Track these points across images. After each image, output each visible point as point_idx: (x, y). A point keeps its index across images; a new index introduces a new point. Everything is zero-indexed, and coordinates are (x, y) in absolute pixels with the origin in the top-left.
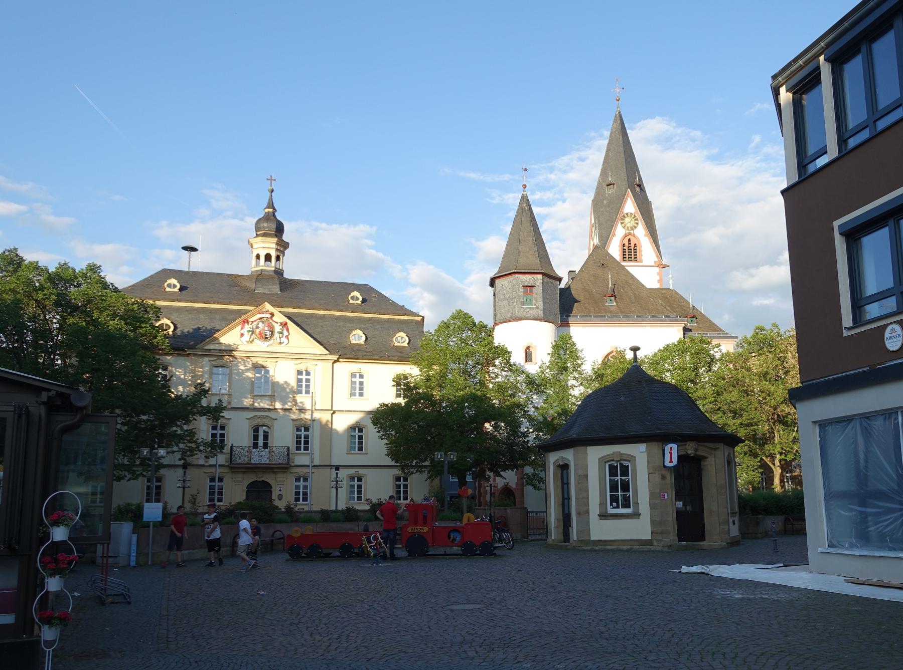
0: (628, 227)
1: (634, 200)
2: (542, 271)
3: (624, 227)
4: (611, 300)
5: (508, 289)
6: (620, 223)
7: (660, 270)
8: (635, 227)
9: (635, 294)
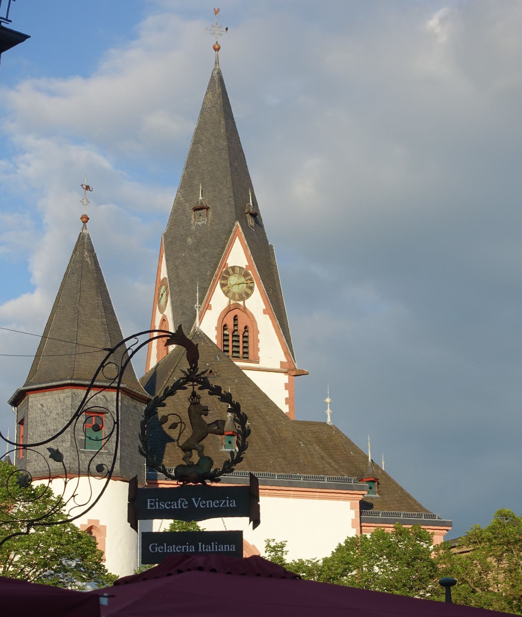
0: (234, 294)
1: (246, 242)
3: (226, 294)
4: (230, 442)
5: (54, 415)
6: (219, 285)
8: (248, 295)
9: (271, 433)
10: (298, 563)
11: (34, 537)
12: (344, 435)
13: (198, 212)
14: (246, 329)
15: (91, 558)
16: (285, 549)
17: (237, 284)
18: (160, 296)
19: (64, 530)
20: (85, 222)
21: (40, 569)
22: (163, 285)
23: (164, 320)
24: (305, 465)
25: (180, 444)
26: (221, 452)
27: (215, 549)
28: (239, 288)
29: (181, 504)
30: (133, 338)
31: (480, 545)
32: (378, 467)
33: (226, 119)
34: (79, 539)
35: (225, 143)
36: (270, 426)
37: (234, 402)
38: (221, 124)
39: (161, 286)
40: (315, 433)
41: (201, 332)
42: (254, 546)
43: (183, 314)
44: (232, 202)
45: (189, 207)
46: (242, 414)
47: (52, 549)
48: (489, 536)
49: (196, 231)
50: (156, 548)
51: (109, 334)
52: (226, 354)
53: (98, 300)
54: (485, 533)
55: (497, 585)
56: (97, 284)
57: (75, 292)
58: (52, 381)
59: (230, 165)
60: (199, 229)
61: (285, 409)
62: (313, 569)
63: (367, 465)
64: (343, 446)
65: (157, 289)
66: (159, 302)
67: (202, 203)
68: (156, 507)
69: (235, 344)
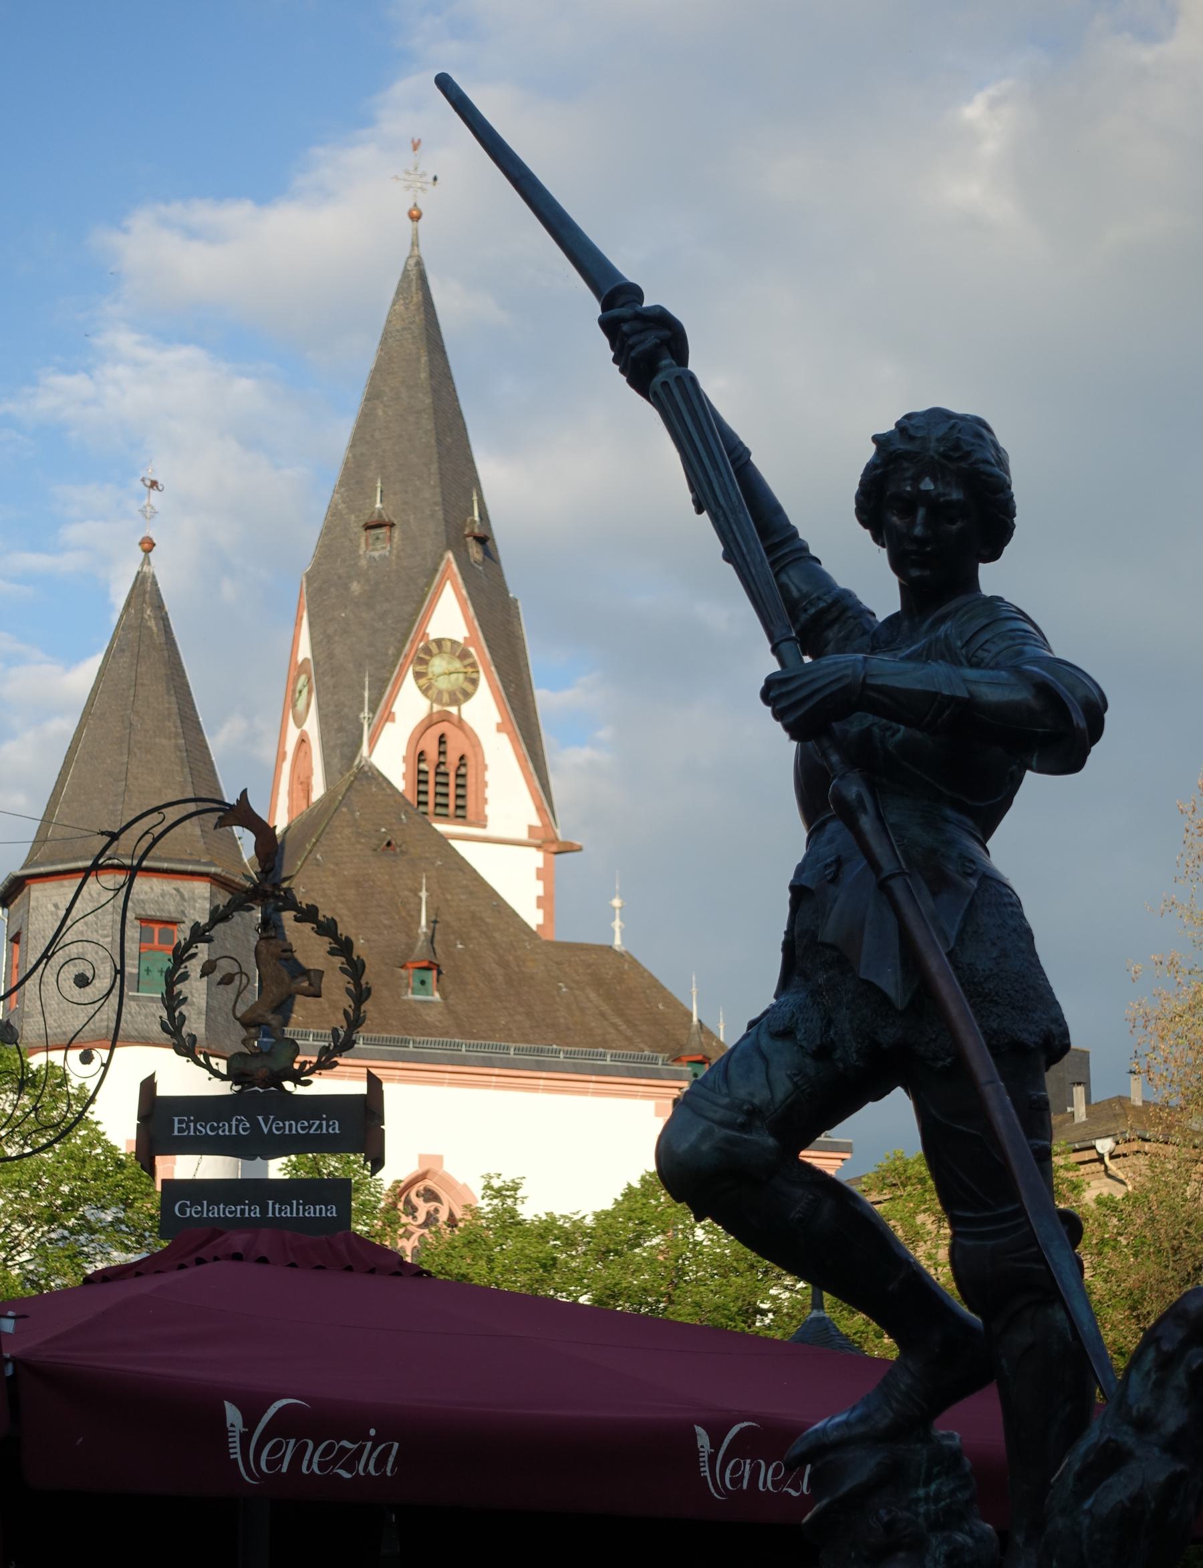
0: (440, 692)
1: (464, 592)
2: (213, 870)
3: (425, 691)
4: (423, 983)
7: (546, 861)
8: (467, 695)
9: (503, 964)
10: (546, 1221)
11: (31, 1164)
12: (645, 970)
13: (374, 532)
14: (463, 762)
15: (141, 1208)
16: (520, 1193)
17: (445, 674)
18: (297, 695)
19: (90, 1152)
20: (147, 551)
21: (42, 1227)
22: (303, 673)
23: (303, 740)
24: (569, 1029)
25: (239, 1015)
26: (404, 1002)
27: (298, 1213)
28: (450, 681)
29: (237, 1126)
30: (156, 814)
31: (905, 1190)
32: (710, 1035)
33: (430, 352)
34: (119, 1169)
35: (428, 401)
36: (501, 951)
37: (341, 935)
38: (420, 362)
39: (299, 676)
40: (589, 966)
41: (372, 767)
42: (465, 1186)
43: (341, 729)
44: (440, 514)
45: (355, 521)
46: (355, 959)
47: (65, 1189)
48: (921, 1173)
49: (368, 568)
50: (188, 1210)
51: (190, 768)
52: (422, 808)
53: (170, 703)
54: (913, 1168)
55: (936, 1269)
56: (169, 672)
57: (125, 686)
58: (75, 859)
59: (438, 443)
60: (375, 564)
61: (533, 917)
62: (574, 1233)
63: (689, 1029)
64: (644, 992)
65: (291, 681)
66: (294, 706)
67: (380, 515)
68: (189, 1132)
69: (441, 789)
